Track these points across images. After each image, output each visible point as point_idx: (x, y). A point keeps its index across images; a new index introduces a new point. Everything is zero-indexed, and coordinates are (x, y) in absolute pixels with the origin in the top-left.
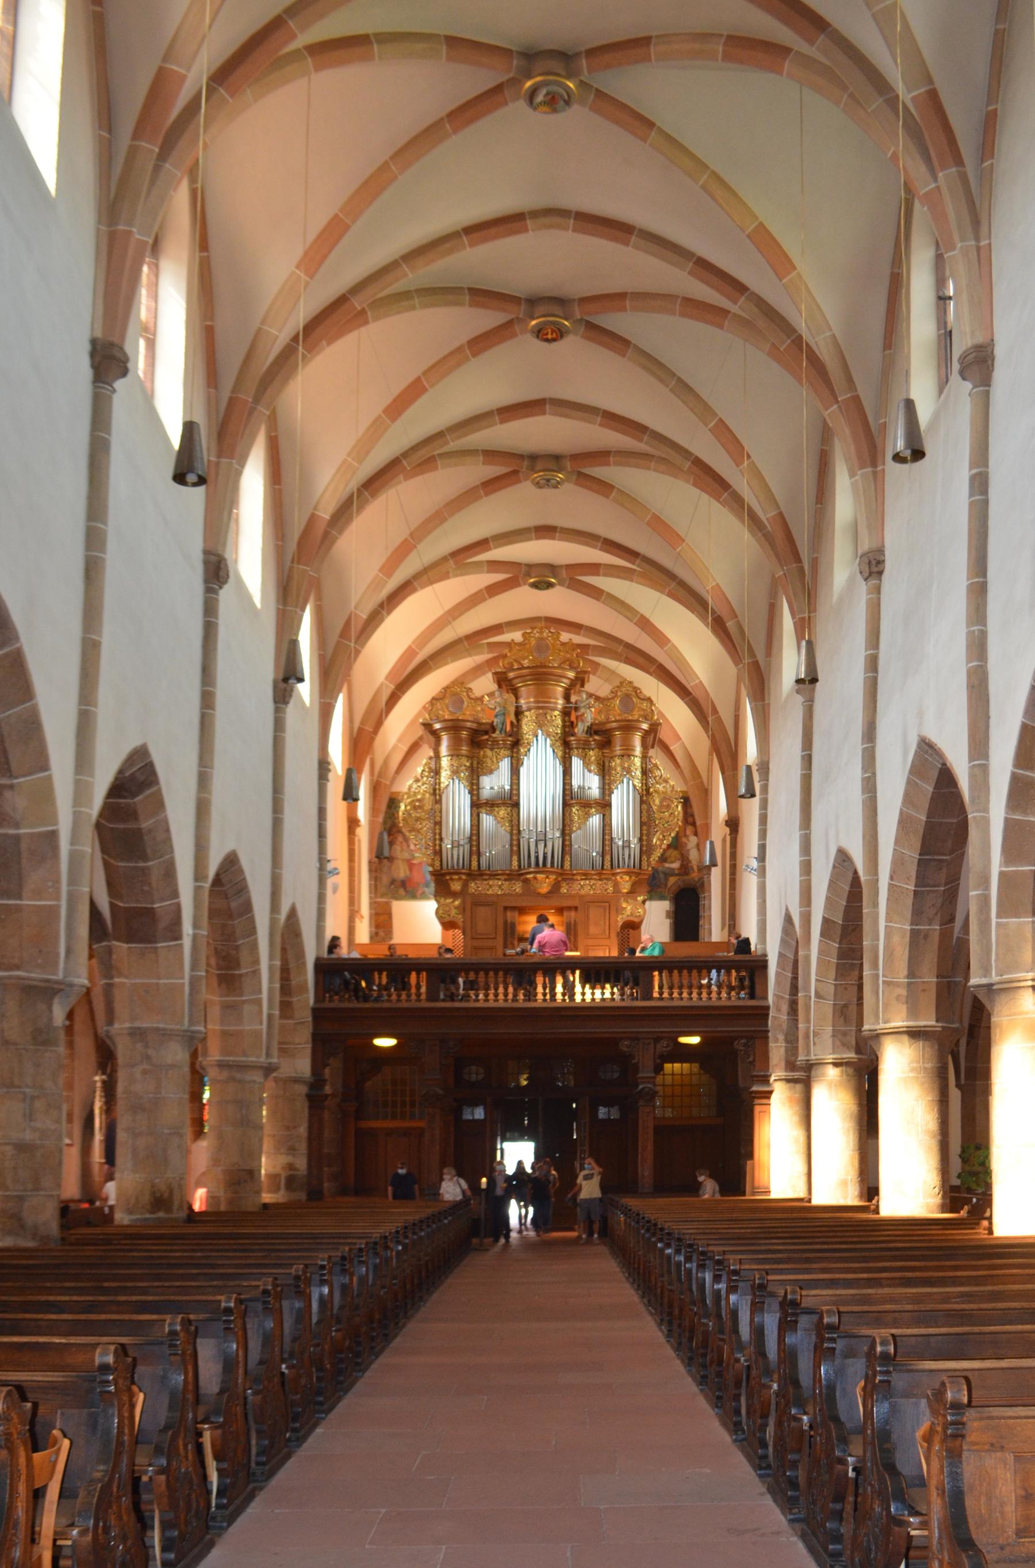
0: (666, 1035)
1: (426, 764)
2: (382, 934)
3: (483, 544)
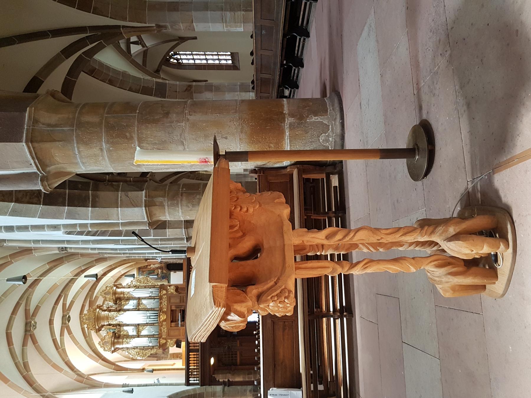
2: (180, 356)
3: (54, 341)
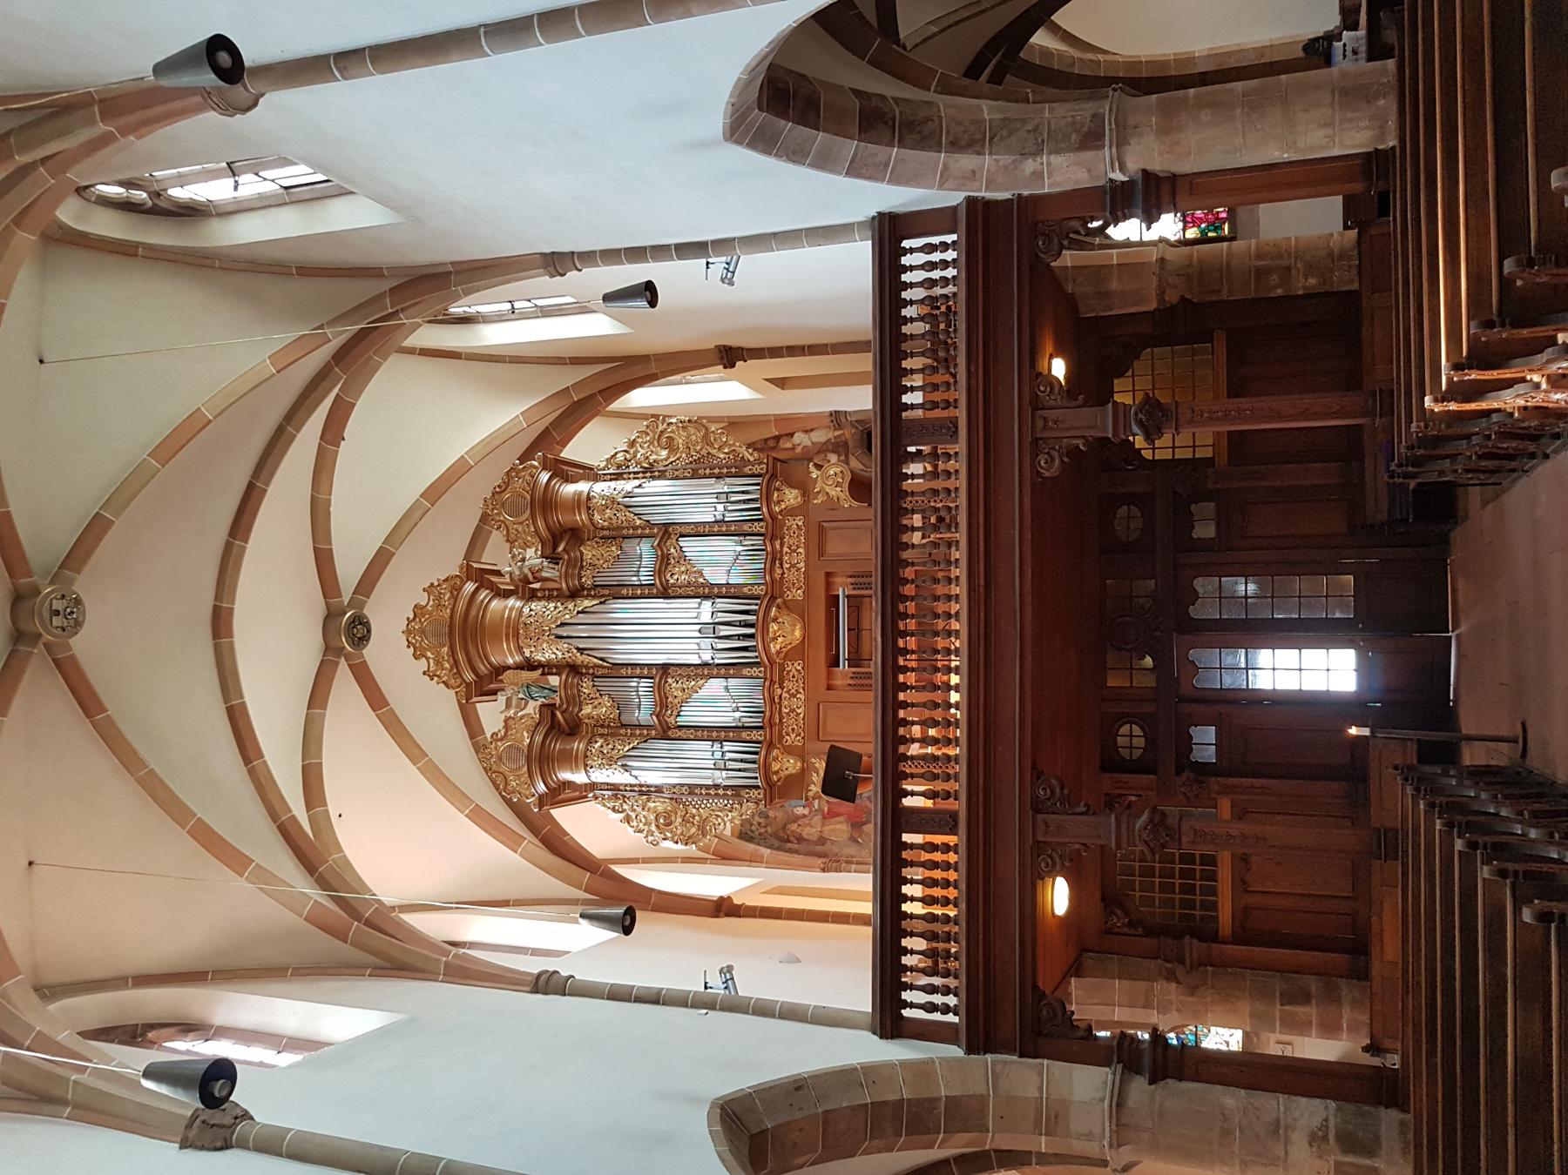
0: (1026, 388)
1: (604, 805)
